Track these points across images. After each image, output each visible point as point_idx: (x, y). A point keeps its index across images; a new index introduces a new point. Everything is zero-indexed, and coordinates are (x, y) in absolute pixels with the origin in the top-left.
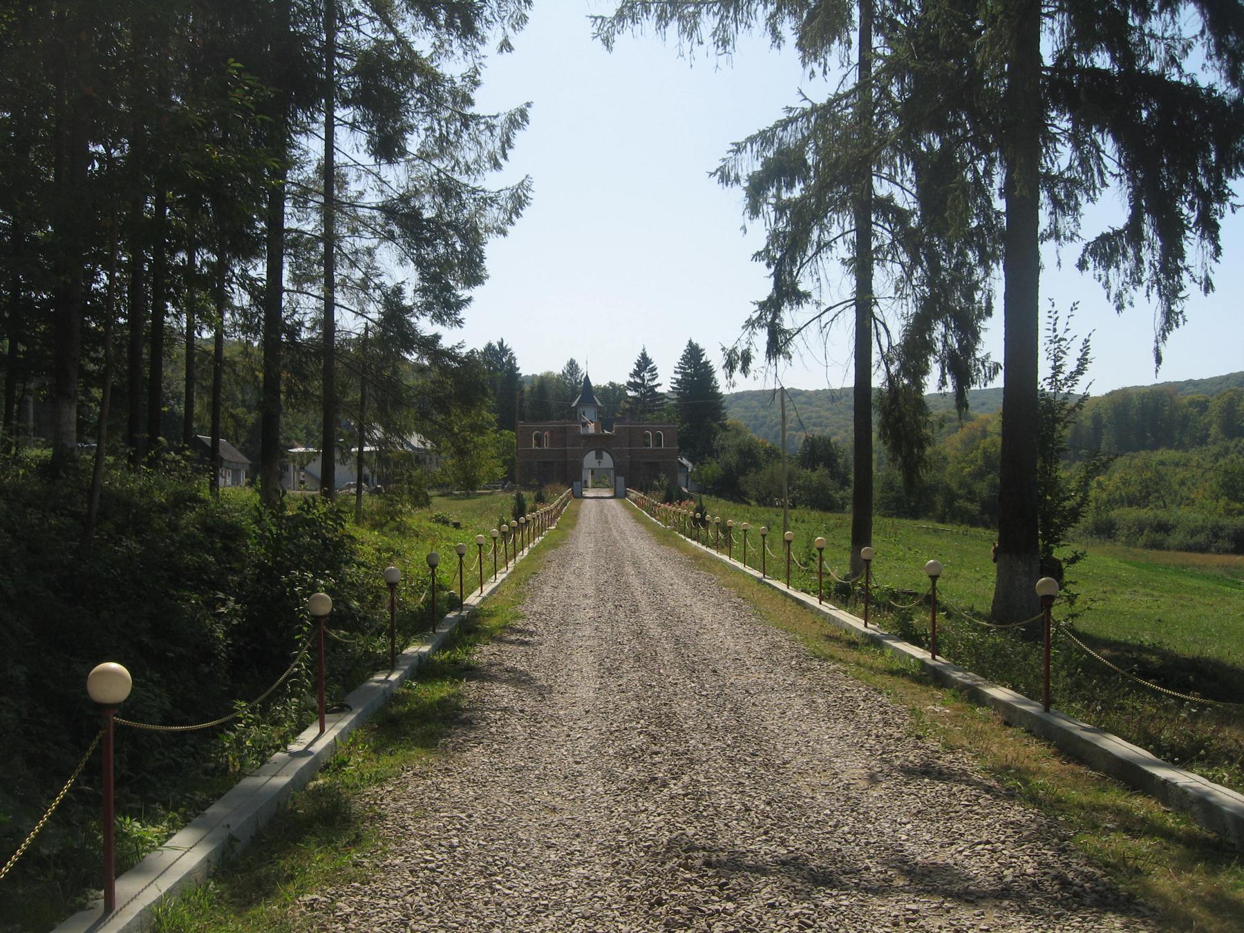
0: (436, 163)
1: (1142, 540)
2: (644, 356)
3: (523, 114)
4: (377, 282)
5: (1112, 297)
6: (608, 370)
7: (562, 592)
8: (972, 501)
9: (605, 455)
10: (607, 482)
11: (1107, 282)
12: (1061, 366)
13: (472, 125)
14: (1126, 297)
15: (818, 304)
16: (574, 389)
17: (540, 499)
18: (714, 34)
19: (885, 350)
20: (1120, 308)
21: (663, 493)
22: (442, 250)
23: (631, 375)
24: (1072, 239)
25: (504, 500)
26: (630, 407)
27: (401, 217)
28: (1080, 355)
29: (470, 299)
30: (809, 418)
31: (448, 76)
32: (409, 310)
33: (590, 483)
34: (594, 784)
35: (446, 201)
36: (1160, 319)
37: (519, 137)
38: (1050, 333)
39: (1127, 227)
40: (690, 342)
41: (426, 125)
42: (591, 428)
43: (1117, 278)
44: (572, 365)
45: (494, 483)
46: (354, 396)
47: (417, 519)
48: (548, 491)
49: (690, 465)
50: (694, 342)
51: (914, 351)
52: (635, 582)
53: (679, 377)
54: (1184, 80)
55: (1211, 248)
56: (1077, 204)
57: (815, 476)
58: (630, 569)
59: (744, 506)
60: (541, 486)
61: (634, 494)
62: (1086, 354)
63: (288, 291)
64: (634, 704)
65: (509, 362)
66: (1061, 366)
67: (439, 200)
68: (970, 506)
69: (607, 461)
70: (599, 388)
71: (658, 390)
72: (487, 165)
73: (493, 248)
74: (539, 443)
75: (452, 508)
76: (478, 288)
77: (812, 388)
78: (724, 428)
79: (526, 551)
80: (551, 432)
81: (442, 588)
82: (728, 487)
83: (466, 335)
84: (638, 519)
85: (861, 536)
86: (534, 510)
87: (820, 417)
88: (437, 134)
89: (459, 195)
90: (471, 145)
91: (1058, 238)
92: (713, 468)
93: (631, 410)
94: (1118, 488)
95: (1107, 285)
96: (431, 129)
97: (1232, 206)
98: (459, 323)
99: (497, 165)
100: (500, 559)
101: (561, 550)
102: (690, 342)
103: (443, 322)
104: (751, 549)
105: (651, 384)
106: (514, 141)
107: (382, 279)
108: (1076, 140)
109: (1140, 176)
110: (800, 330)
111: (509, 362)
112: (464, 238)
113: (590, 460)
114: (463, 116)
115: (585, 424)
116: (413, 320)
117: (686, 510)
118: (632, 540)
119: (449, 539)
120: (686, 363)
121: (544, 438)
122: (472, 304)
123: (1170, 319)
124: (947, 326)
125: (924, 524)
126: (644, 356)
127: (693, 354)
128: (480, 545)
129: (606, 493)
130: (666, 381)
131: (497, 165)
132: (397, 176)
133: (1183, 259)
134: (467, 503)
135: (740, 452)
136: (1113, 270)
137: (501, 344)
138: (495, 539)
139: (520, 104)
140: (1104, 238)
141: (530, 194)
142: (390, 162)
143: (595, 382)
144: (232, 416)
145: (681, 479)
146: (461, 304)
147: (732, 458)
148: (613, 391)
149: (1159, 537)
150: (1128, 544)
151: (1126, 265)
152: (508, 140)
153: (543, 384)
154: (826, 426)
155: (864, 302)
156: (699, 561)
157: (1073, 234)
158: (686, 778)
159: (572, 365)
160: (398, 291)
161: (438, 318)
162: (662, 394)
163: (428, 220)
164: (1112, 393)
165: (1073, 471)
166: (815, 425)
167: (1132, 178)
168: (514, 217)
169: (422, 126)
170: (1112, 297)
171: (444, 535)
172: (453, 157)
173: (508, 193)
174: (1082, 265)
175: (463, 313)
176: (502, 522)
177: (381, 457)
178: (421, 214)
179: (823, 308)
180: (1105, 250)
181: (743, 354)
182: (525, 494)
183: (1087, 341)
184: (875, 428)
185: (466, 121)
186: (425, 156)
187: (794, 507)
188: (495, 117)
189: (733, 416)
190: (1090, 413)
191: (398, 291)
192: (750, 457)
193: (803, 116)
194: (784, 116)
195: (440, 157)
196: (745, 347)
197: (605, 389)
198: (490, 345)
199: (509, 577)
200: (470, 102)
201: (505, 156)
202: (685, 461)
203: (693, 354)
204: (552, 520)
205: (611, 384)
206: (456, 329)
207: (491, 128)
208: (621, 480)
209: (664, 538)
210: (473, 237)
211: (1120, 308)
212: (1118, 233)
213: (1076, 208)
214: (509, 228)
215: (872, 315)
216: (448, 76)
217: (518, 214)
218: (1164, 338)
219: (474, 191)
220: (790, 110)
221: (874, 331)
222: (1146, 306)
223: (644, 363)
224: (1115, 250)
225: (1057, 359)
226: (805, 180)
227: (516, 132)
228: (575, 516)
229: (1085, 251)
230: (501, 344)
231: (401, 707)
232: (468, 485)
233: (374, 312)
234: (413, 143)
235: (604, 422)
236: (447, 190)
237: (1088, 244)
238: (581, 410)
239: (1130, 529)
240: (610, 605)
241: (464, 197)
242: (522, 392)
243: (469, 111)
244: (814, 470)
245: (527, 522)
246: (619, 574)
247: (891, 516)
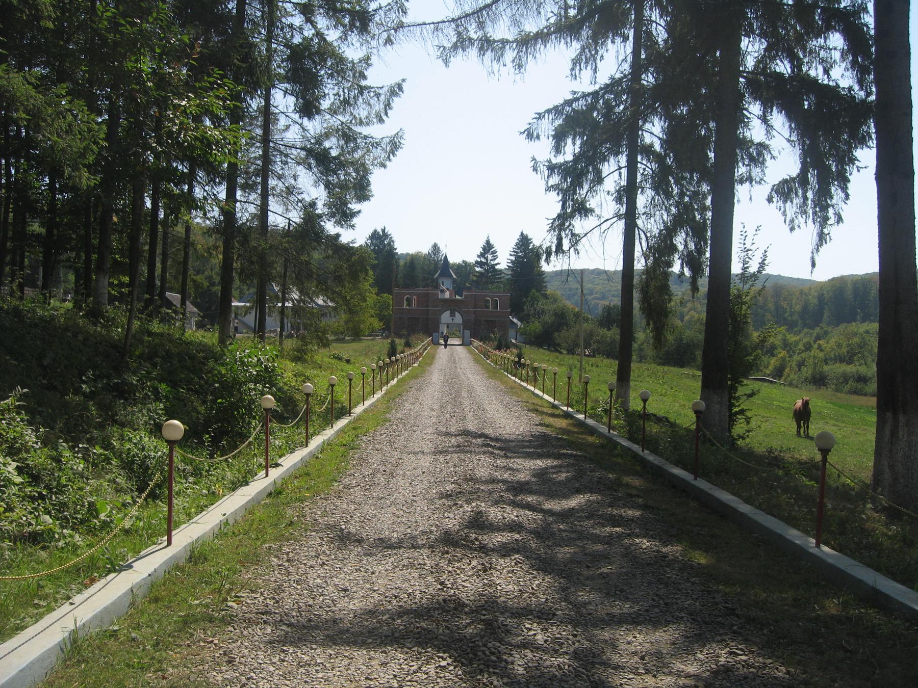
0: (340, 117)
1: (847, 388)
2: (488, 242)
3: (400, 87)
4: (300, 198)
5: (787, 221)
6: (461, 251)
7: (417, 407)
9: (457, 314)
11: (785, 211)
12: (747, 268)
13: (366, 92)
14: (796, 222)
15: (599, 217)
16: (436, 263)
17: (408, 345)
18: (513, 61)
19: (644, 249)
20: (792, 229)
21: (496, 343)
22: (342, 178)
23: (479, 256)
24: (760, 183)
25: (381, 344)
26: (477, 278)
27: (318, 157)
28: (760, 261)
29: (359, 212)
30: (609, 291)
31: (350, 59)
32: (320, 216)
34: (422, 505)
35: (346, 143)
36: (815, 238)
37: (396, 102)
38: (742, 246)
39: (798, 175)
40: (522, 234)
41: (335, 92)
42: (447, 295)
43: (791, 208)
44: (435, 247)
45: (373, 334)
46: (279, 268)
47: (322, 355)
48: (413, 339)
49: (519, 323)
50: (525, 233)
51: (662, 249)
52: (466, 402)
53: (513, 258)
54: (831, 83)
55: (843, 195)
56: (764, 160)
57: (609, 333)
58: (464, 394)
59: (557, 354)
60: (409, 335)
61: (476, 343)
62: (764, 260)
63: (241, 201)
64: (452, 469)
65: (389, 244)
66: (747, 268)
67: (342, 142)
69: (458, 319)
70: (454, 264)
71: (497, 267)
72: (375, 120)
73: (377, 179)
74: (409, 304)
75: (346, 350)
76: (366, 203)
78: (546, 297)
79: (395, 380)
81: (337, 402)
82: (545, 340)
83: (355, 235)
84: (476, 360)
85: (623, 376)
86: (403, 352)
88: (342, 99)
89: (355, 139)
90: (364, 106)
91: (751, 182)
92: (536, 326)
93: (476, 282)
94: (833, 349)
95: (784, 214)
96: (338, 94)
97: (858, 167)
98: (353, 226)
99: (381, 120)
100: (377, 383)
101: (420, 380)
102: (522, 234)
103: (342, 226)
104: (548, 383)
105: (493, 263)
106: (393, 105)
107: (303, 196)
108: (764, 119)
109: (807, 142)
110: (586, 235)
111: (389, 244)
112: (357, 171)
113: (446, 317)
114: (360, 86)
115: (443, 291)
116: (322, 223)
117: (510, 355)
118: (470, 376)
119: (342, 370)
120: (518, 248)
121: (412, 299)
122: (361, 214)
123: (822, 238)
124: (687, 235)
125: (686, 371)
126: (488, 242)
127: (524, 241)
128: (363, 374)
130: (503, 260)
131: (381, 120)
132: (314, 126)
133: (831, 198)
134: (355, 345)
135: (556, 314)
136: (789, 203)
137: (383, 231)
138: (373, 370)
139: (398, 79)
140: (785, 182)
141: (402, 141)
142: (309, 119)
143: (451, 260)
144: (194, 281)
145: (512, 333)
146: (353, 214)
147: (548, 318)
148: (464, 269)
149: (860, 386)
150: (837, 390)
151: (797, 201)
152: (389, 104)
153: (413, 261)
155: (630, 218)
156: (513, 390)
157: (761, 179)
158: (474, 504)
159: (435, 247)
160: (313, 204)
161: (338, 223)
162: (501, 270)
163: (334, 158)
164: (833, 279)
165: (802, 335)
167: (804, 144)
168: (391, 156)
169: (331, 93)
170: (787, 221)
171: (339, 368)
172: (352, 114)
173: (388, 140)
174: (770, 200)
175: (355, 221)
176: (379, 359)
177: (296, 310)
178: (330, 153)
179: (603, 220)
180: (784, 191)
181: (547, 248)
182: (397, 341)
183: (766, 251)
184: (636, 304)
185: (362, 90)
186: (333, 111)
187: (594, 356)
188: (381, 88)
189: (552, 288)
190: (816, 294)
191: (313, 204)
192: (562, 319)
193: (583, 97)
194: (570, 97)
195: (344, 112)
196: (549, 245)
197: (459, 266)
198: (375, 231)
199: (383, 397)
200: (365, 77)
201: (386, 114)
202: (515, 320)
203: (524, 241)
204: (415, 360)
205: (464, 261)
206: (350, 231)
207: (378, 95)
208: (467, 333)
209: (492, 374)
210: (363, 172)
211: (792, 229)
212: (793, 180)
213: (763, 163)
214: (388, 163)
215: (636, 225)
216: (350, 59)
217: (394, 154)
218: (818, 250)
219: (366, 137)
220: (574, 93)
221: (637, 236)
222: (808, 230)
223: (488, 248)
224: (790, 190)
225: (745, 263)
226: (592, 131)
227: (395, 98)
228: (432, 357)
229: (772, 190)
230: (383, 231)
231: (371, 280)
232: (357, 335)
233: (296, 216)
234: (325, 104)
235: (458, 290)
236: (348, 136)
237: (774, 186)
238: (440, 281)
239: (838, 379)
240: (447, 416)
241: (359, 141)
242: (398, 266)
243: (363, 83)
244: (609, 329)
245: (397, 360)
246: (458, 395)
247: (664, 364)
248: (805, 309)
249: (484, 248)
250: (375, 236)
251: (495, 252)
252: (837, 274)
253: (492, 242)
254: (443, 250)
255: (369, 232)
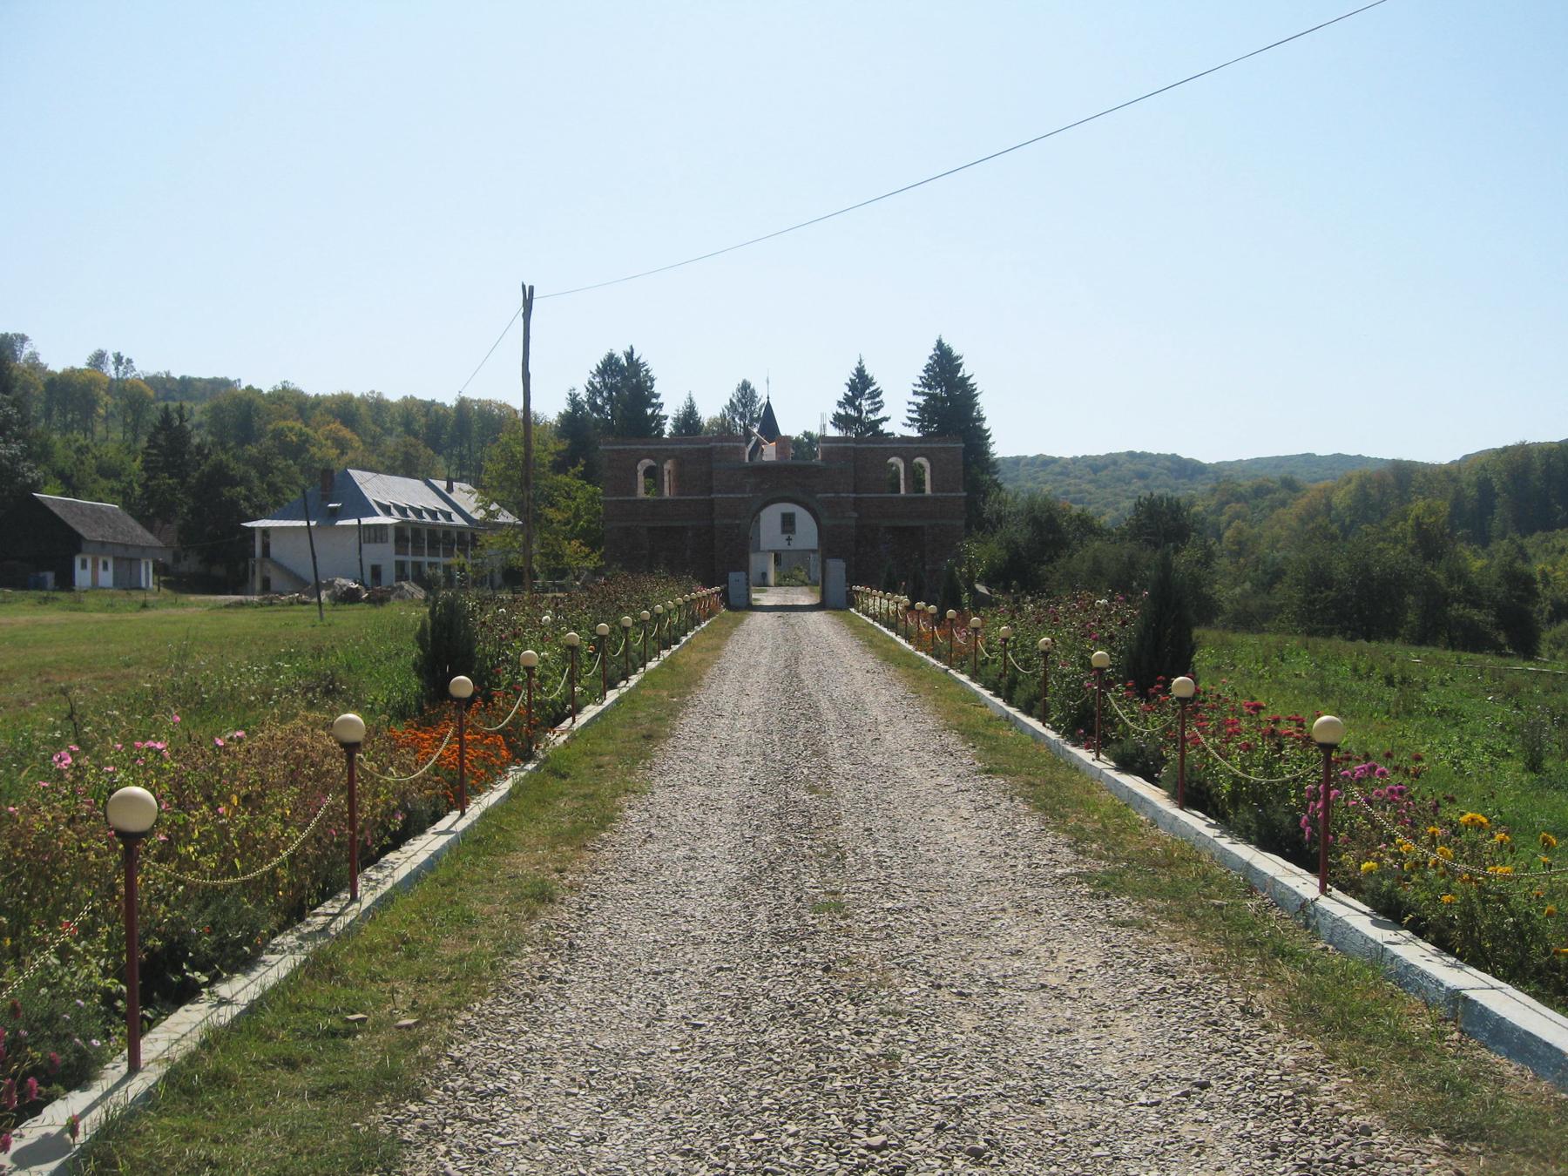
2: (860, 372)
8: (1476, 605)
10: (802, 576)
23: (840, 404)
30: (1067, 493)
33: (772, 579)
61: (880, 602)
68: (1477, 615)
71: (885, 427)
77: (1068, 455)
80: (680, 464)
87: (1081, 492)
105: (872, 417)
126: (860, 372)
129: (804, 597)
130: (898, 416)
137: (630, 356)
147: (1021, 533)
154: (1090, 504)
166: (1074, 501)
190: (1474, 479)
198: (611, 356)
208: (837, 567)
223: (861, 384)
230: (630, 356)
248: (1457, 504)
249: (853, 387)
250: (610, 366)
251: (877, 393)
252: (1511, 441)
253: (869, 372)
254: (761, 394)
255: (597, 359)
